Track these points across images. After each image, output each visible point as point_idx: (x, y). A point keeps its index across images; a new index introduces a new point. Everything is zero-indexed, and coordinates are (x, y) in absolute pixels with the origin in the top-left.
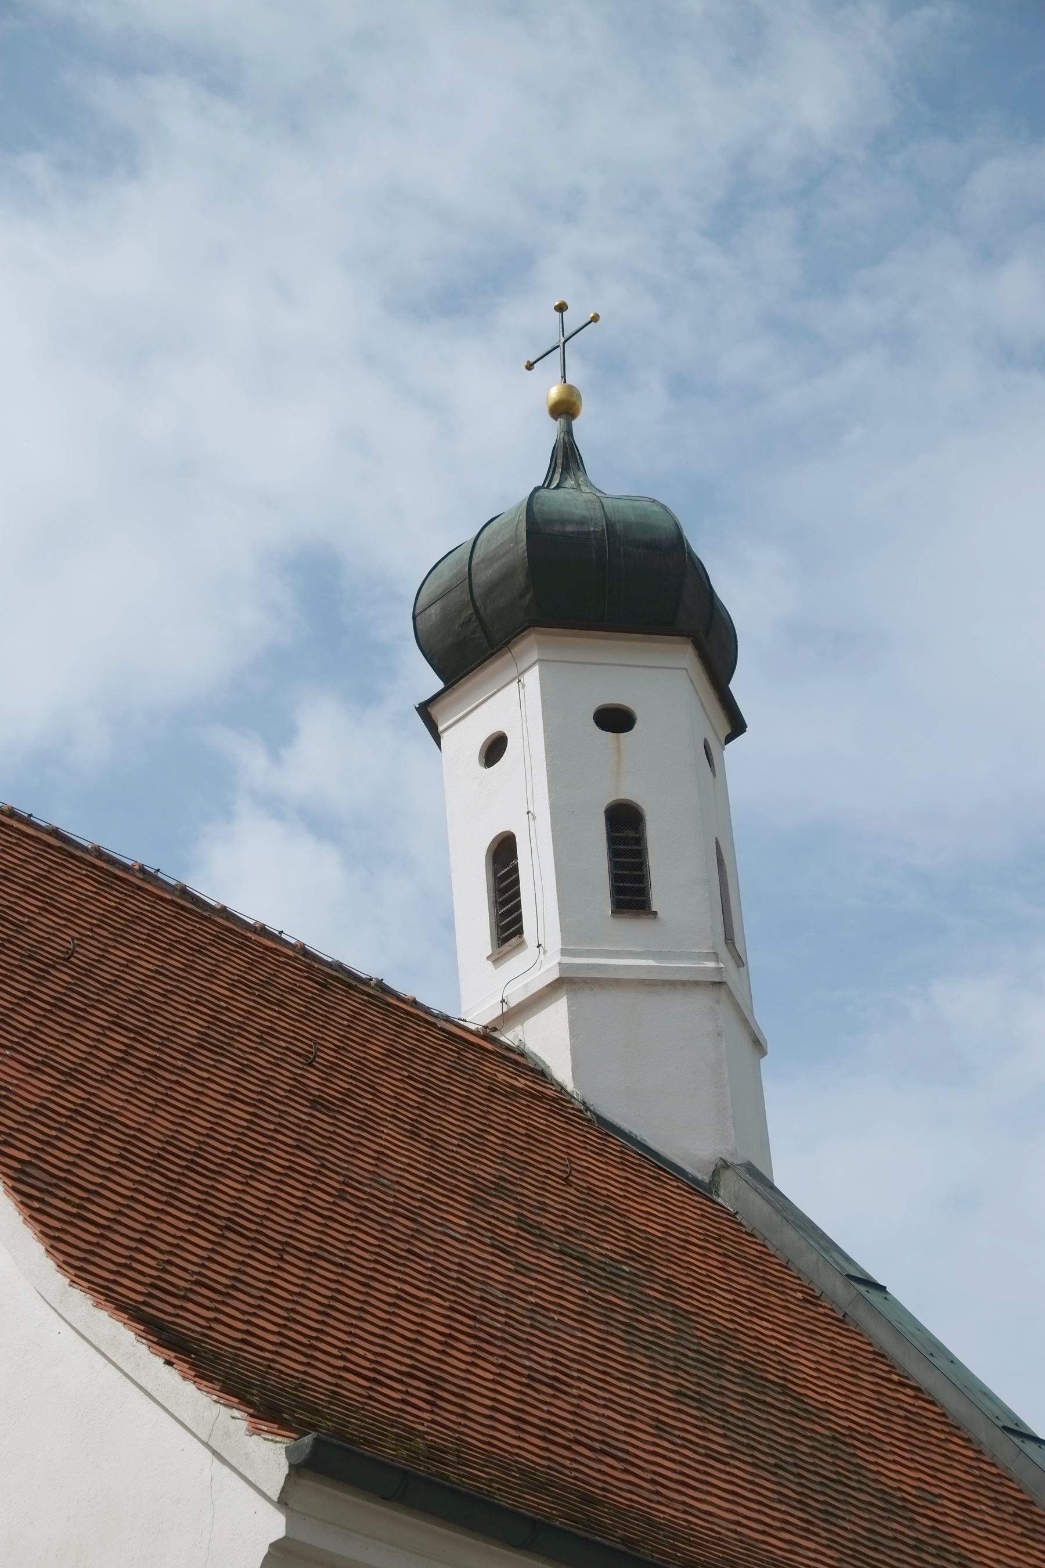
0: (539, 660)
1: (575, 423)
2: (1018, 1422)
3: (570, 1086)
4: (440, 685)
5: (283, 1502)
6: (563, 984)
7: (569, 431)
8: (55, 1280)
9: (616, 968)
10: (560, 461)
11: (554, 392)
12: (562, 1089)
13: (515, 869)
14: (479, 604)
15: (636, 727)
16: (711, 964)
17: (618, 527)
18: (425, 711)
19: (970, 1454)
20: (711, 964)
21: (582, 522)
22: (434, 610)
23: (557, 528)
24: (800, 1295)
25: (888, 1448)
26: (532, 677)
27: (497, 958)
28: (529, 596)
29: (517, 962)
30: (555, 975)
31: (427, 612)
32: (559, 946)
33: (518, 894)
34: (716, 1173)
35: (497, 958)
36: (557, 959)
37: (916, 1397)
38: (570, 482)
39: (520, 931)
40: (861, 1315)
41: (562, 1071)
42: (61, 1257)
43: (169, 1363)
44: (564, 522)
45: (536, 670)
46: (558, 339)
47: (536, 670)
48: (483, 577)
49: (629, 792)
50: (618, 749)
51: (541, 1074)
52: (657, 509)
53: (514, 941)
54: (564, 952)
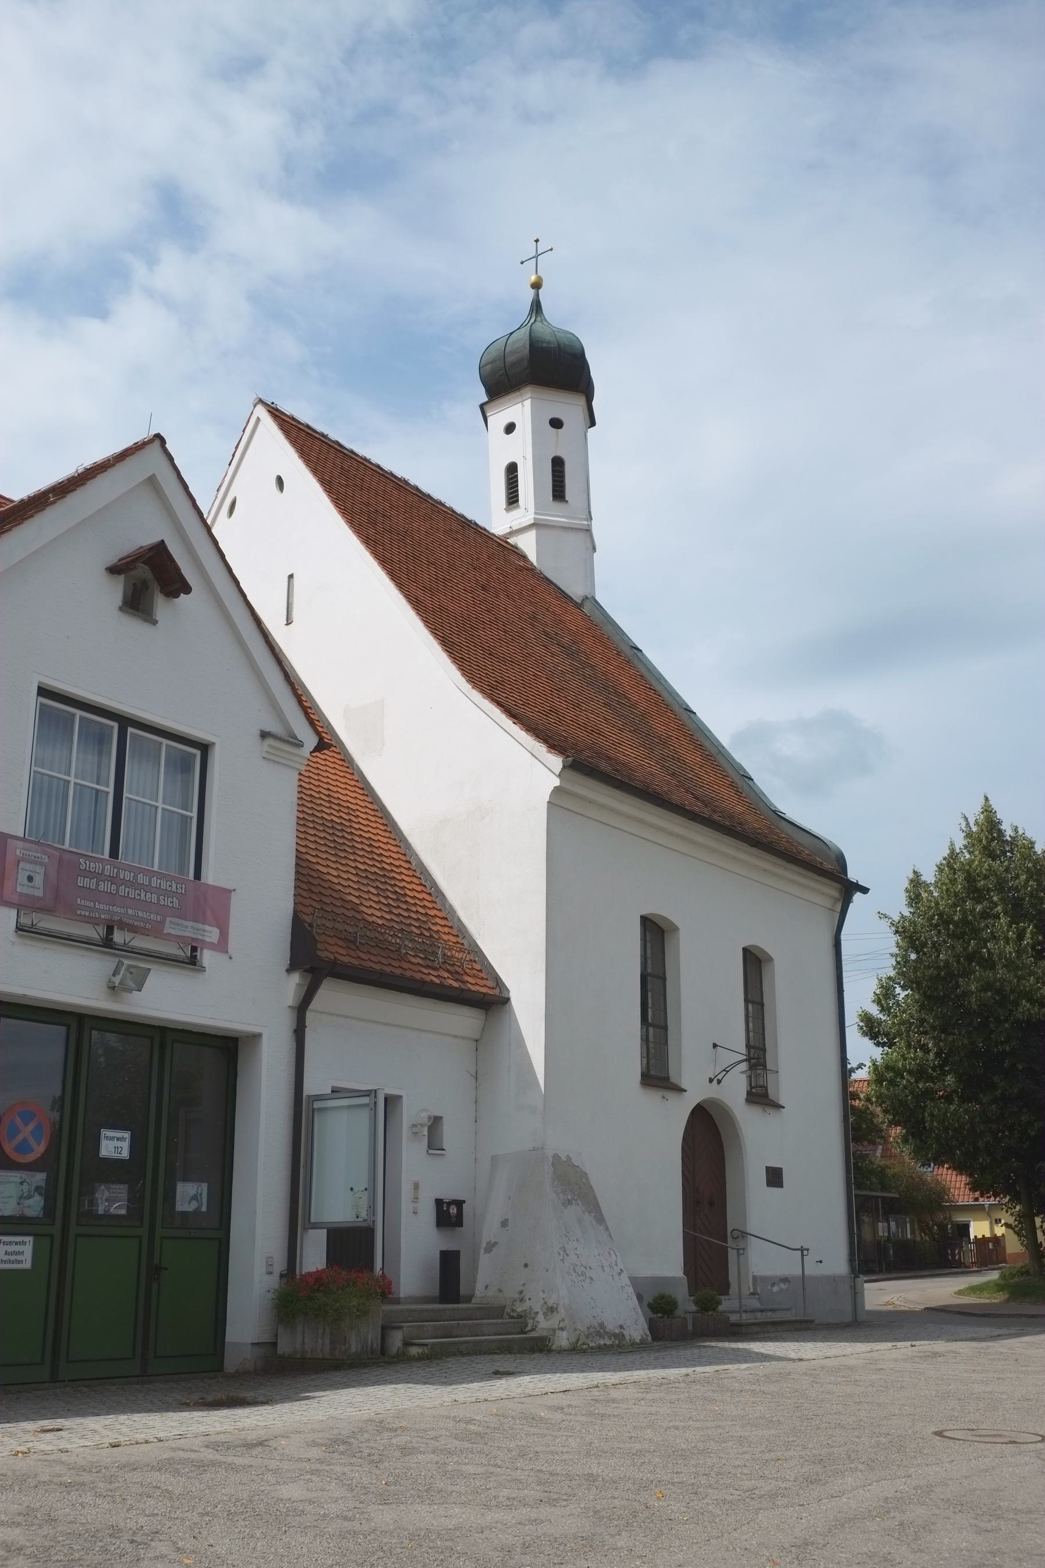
0: (531, 397)
1: (540, 291)
2: (688, 706)
3: (535, 564)
4: (487, 399)
5: (559, 776)
6: (536, 525)
7: (538, 295)
8: (467, 687)
9: (553, 521)
10: (535, 308)
11: (533, 278)
12: (532, 564)
13: (517, 476)
14: (507, 369)
15: (564, 427)
16: (586, 523)
17: (562, 346)
18: (482, 407)
19: (673, 716)
20: (586, 523)
21: (549, 343)
22: (488, 367)
23: (540, 344)
24: (615, 652)
25: (655, 717)
26: (528, 403)
27: (508, 510)
28: (528, 370)
29: (515, 514)
30: (532, 522)
31: (485, 367)
32: (533, 511)
33: (517, 486)
34: (583, 600)
35: (508, 510)
36: (533, 516)
37: (655, 694)
38: (539, 319)
39: (517, 501)
40: (635, 661)
41: (532, 557)
42: (468, 678)
43: (514, 723)
44: (542, 342)
45: (530, 400)
46: (534, 254)
47: (530, 400)
48: (510, 359)
49: (559, 454)
50: (557, 435)
51: (524, 557)
52: (575, 339)
53: (515, 505)
54: (535, 513)
